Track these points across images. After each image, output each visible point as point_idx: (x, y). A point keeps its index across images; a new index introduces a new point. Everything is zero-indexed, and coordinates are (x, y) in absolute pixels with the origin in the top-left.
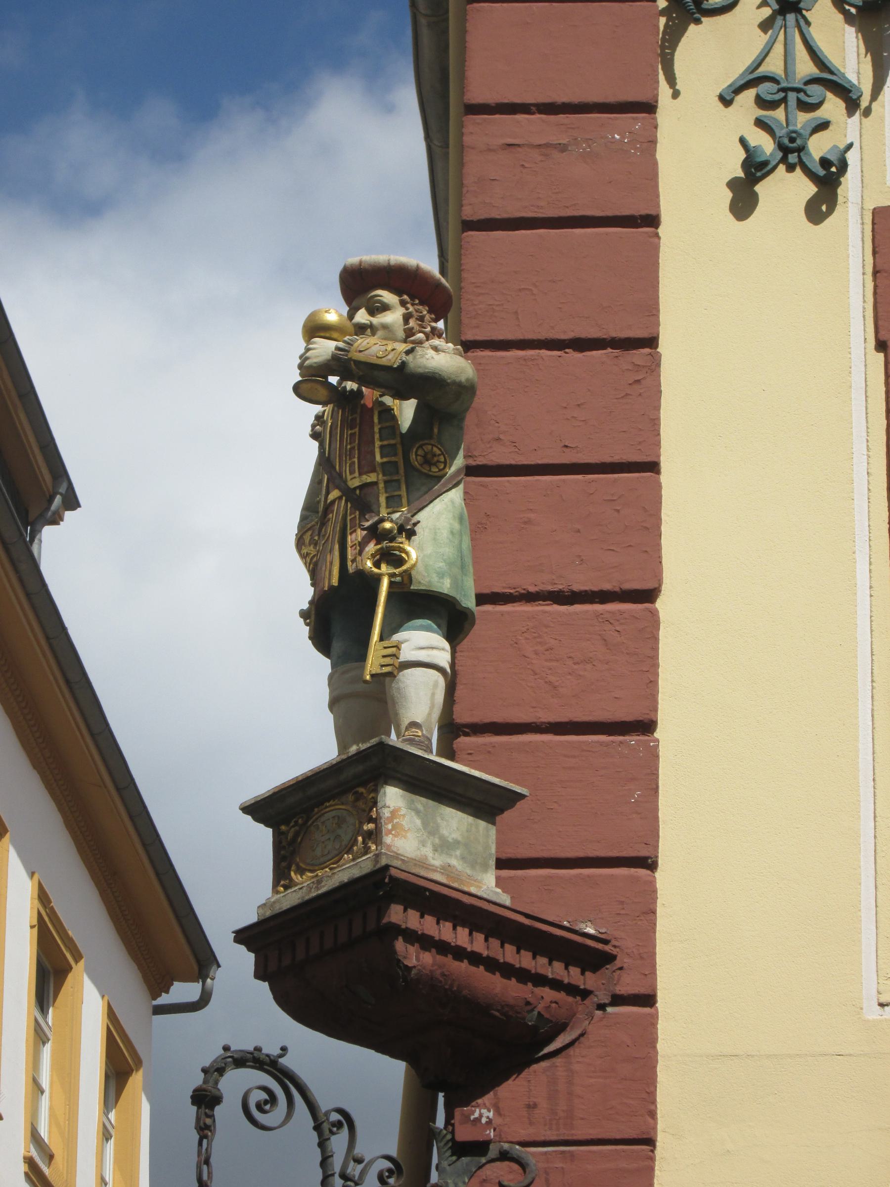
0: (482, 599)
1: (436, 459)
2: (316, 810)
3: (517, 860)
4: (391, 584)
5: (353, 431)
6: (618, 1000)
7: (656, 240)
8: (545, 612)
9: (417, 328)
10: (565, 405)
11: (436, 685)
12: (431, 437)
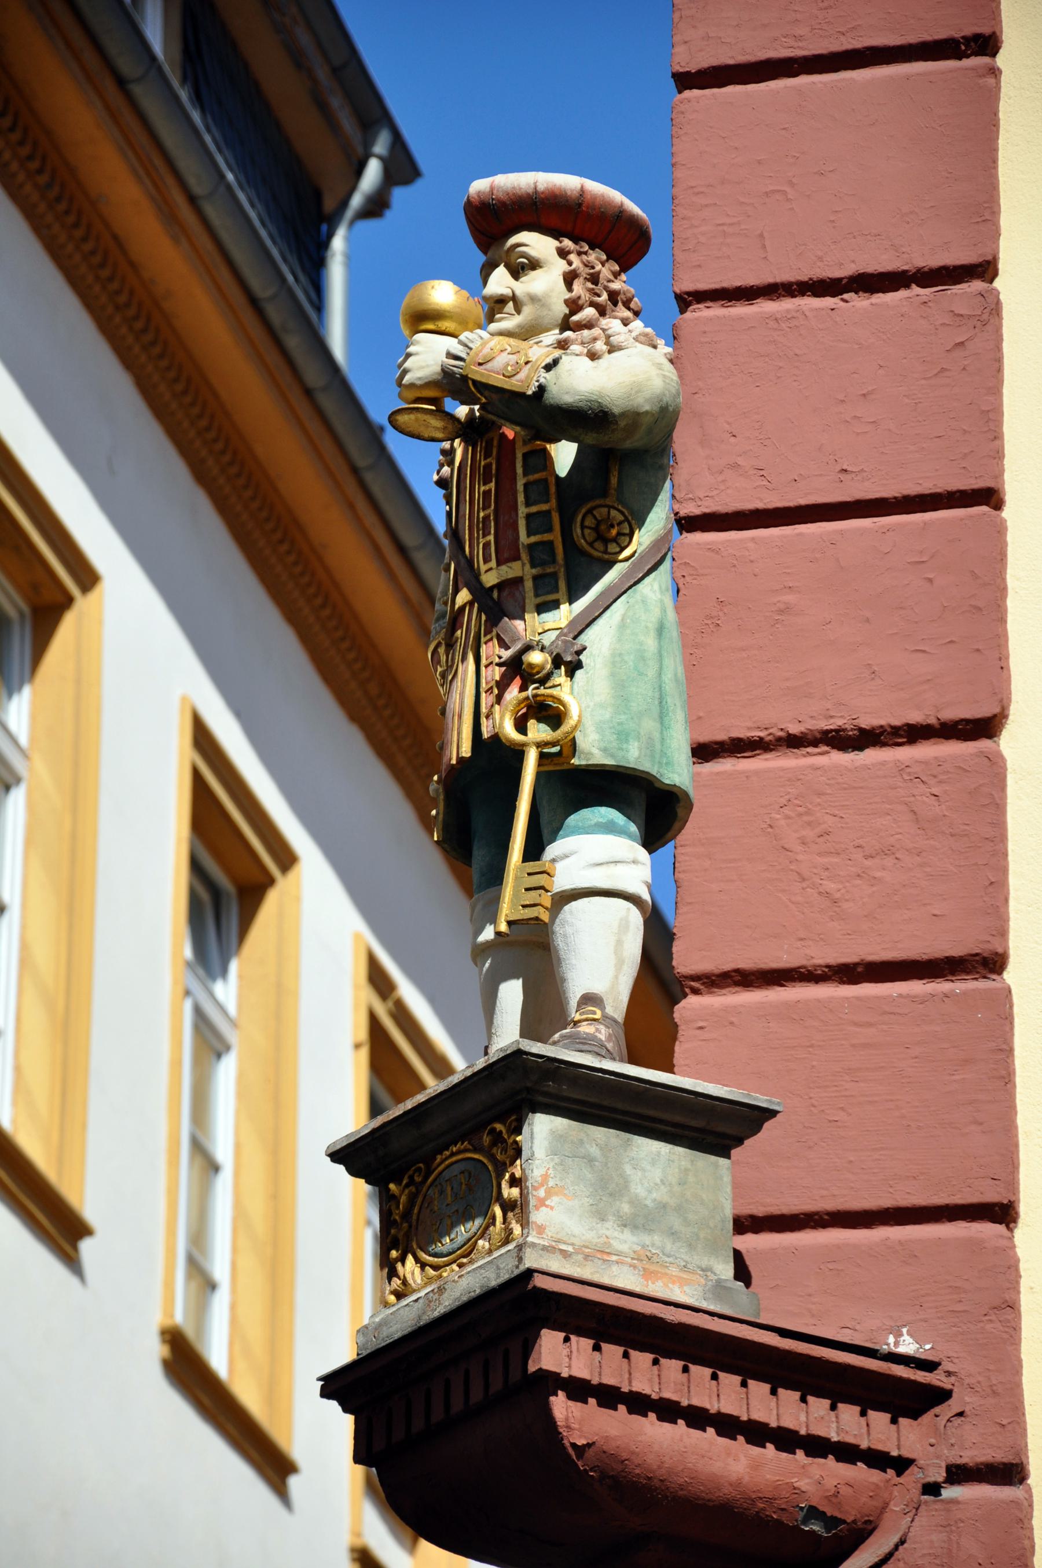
1: (614, 532)
2: (439, 1158)
3: (782, 1217)
4: (542, 757)
5: (487, 488)
7: (991, 81)
9: (585, 296)
10: (841, 397)
11: (624, 926)
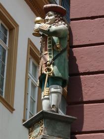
0: (70, 75)
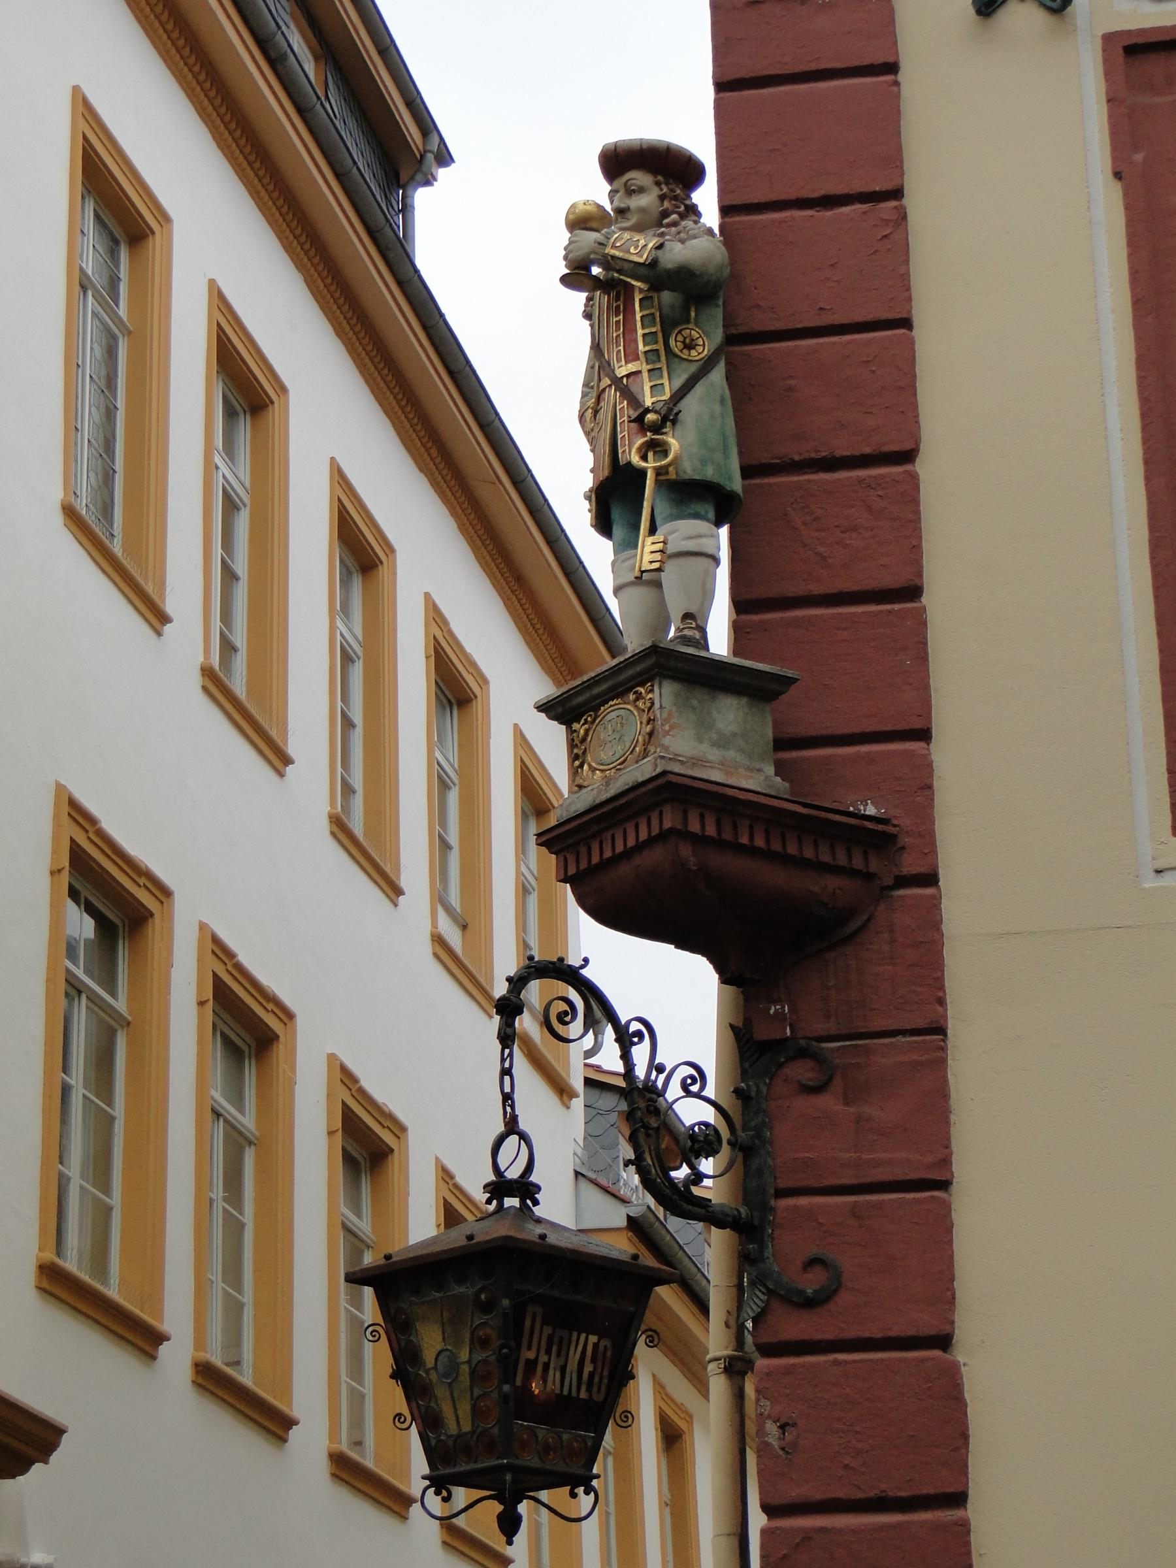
0: (748, 472)
6: (903, 881)
7: (895, 89)
8: (809, 481)
12: (688, 322)
